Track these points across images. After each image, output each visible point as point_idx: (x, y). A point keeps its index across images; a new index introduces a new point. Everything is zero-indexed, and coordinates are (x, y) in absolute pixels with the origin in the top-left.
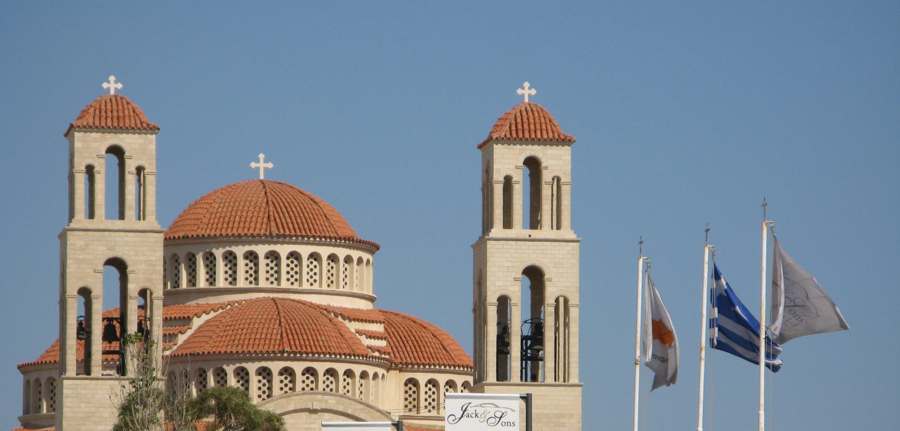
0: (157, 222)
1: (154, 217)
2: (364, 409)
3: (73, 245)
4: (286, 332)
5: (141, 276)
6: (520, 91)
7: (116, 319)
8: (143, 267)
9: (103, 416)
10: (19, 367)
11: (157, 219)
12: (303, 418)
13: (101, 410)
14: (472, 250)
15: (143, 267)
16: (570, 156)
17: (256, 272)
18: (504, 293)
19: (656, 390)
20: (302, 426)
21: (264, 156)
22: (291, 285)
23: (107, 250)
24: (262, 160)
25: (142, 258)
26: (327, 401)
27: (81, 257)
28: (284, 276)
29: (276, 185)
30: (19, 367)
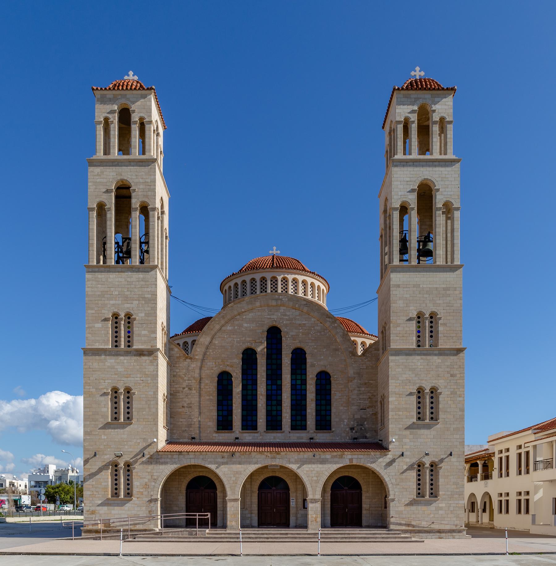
2: (307, 304)
3: (93, 172)
4: (267, 264)
5: (140, 194)
6: (418, 69)
10: (509, 448)
12: (266, 312)
13: (112, 289)
15: (141, 187)
16: (452, 102)
19: (465, 347)
20: (265, 317)
25: (141, 181)
27: (98, 180)
29: (346, 320)
30: (509, 448)
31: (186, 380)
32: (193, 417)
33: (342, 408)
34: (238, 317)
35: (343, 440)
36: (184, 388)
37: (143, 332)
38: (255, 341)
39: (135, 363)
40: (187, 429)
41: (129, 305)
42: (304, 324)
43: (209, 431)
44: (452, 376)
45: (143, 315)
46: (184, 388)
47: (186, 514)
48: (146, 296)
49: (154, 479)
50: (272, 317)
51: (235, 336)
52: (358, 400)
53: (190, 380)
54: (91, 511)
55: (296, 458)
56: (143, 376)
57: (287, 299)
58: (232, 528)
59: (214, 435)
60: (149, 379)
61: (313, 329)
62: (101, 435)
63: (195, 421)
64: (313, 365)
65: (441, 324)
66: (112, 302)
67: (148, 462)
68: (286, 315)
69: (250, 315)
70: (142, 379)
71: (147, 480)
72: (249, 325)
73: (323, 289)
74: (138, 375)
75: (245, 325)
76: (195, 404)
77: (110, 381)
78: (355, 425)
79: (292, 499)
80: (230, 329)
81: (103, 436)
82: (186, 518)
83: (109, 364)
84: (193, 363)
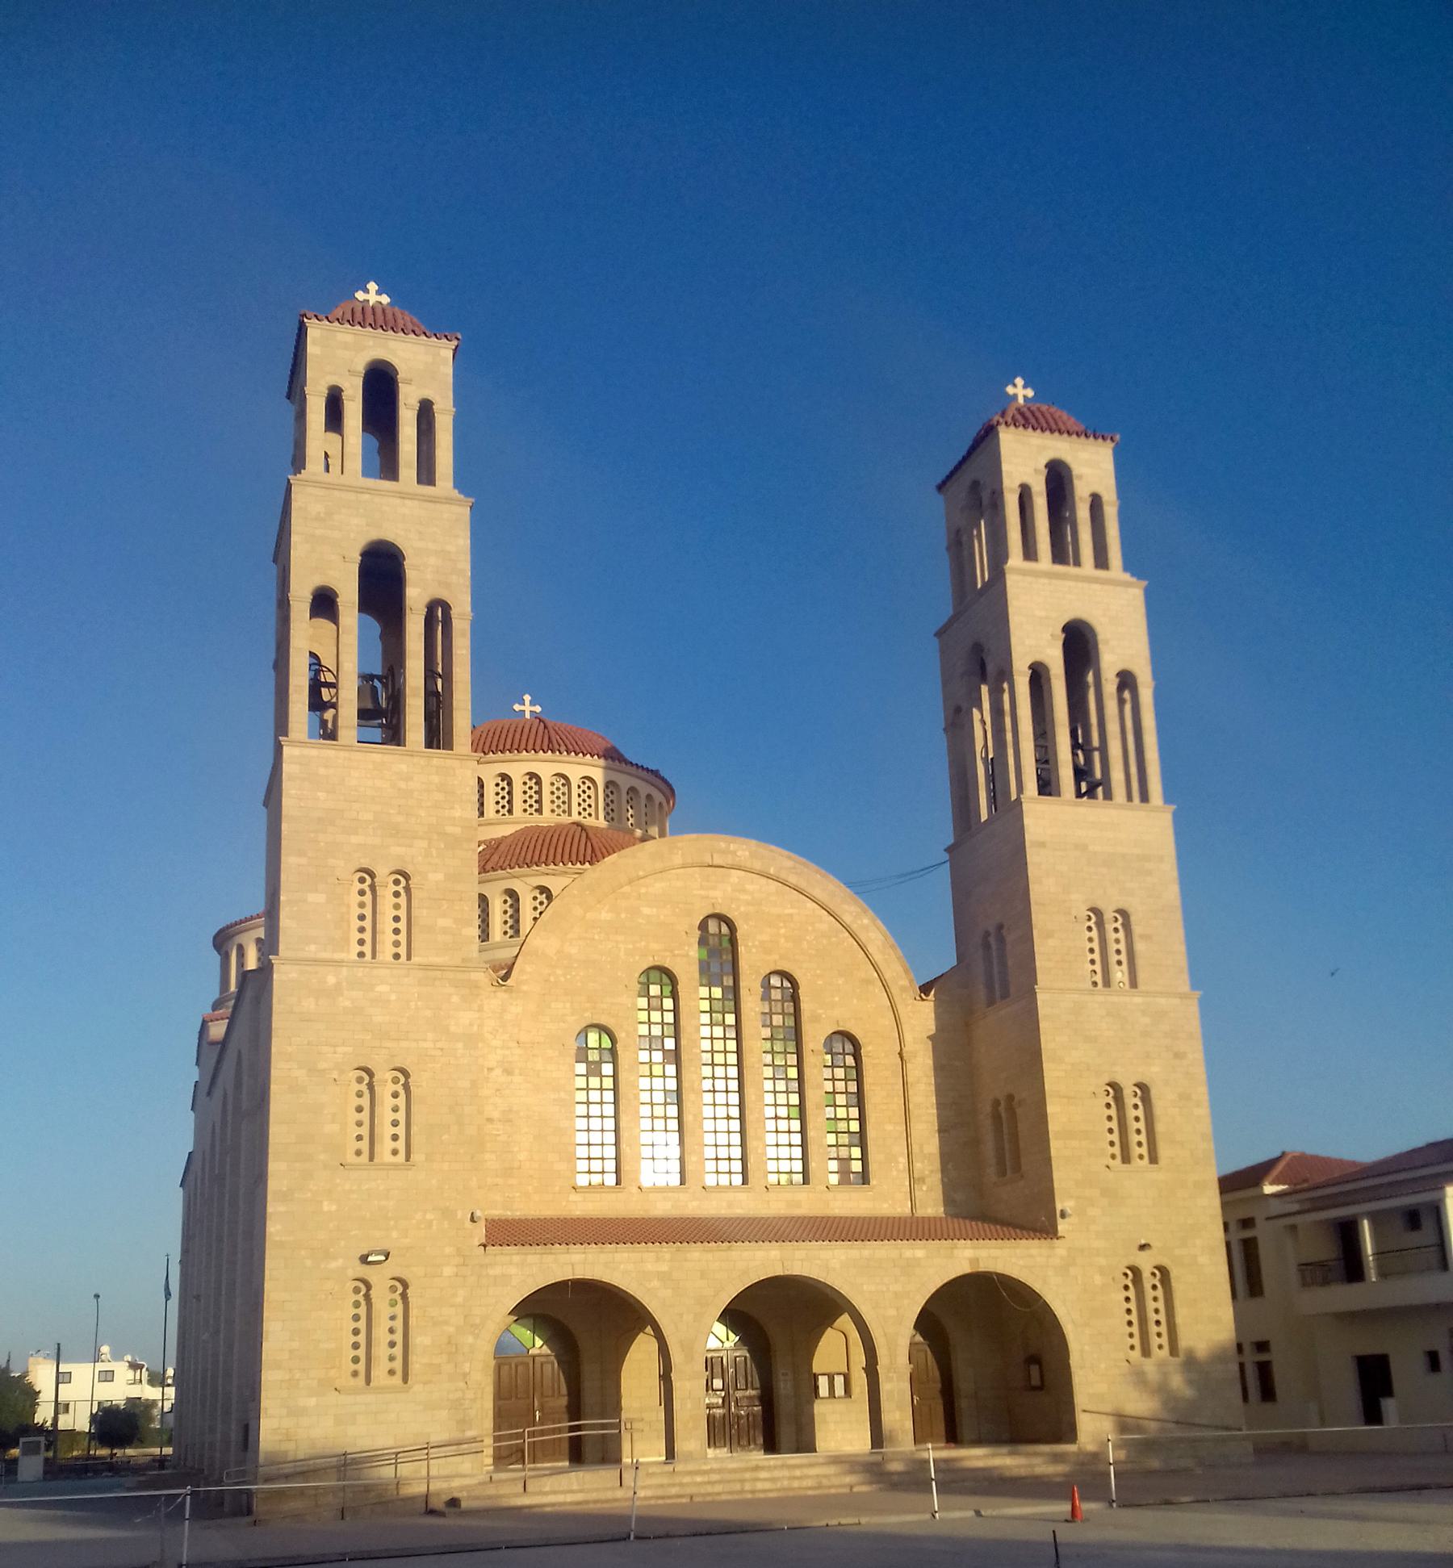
0: (456, 491)
1: (451, 484)
5: (429, 577)
7: (378, 677)
8: (432, 560)
9: (360, 818)
11: (455, 486)
14: (936, 641)
15: (433, 561)
17: (539, 792)
18: (1038, 657)
21: (530, 698)
22: (392, 1157)
23: (367, 525)
24: (527, 702)
26: (734, 853)
27: (318, 532)
28: (575, 809)
31: (496, 1048)
32: (516, 1149)
33: (889, 1127)
34: (627, 889)
35: (899, 1210)
36: (490, 1069)
37: (442, 922)
38: (672, 951)
39: (419, 1003)
40: (500, 1181)
41: (404, 849)
42: (791, 915)
43: (557, 1188)
44: (1178, 1056)
45: (440, 876)
46: (490, 1069)
47: (570, 1427)
48: (450, 829)
49: (472, 1326)
50: (712, 893)
51: (620, 938)
52: (928, 1108)
53: (508, 1048)
54: (284, 1431)
55: (843, 1258)
56: (443, 1039)
57: (747, 853)
58: (689, 1457)
59: (570, 1199)
60: (460, 1045)
61: (810, 928)
62: (321, 1202)
63: (521, 1159)
64: (816, 1019)
65: (1141, 936)
66: (354, 839)
67: (457, 1276)
68: (744, 891)
69: (658, 886)
70: (439, 1045)
71: (452, 1329)
72: (655, 910)
73: (660, 804)
74: (430, 1036)
75: (646, 911)
76: (522, 1114)
77: (350, 1049)
78: (927, 1172)
79: (783, 1374)
80: (608, 919)
81: (325, 1203)
82: (570, 1437)
83: (348, 1003)
84: (515, 1003)
